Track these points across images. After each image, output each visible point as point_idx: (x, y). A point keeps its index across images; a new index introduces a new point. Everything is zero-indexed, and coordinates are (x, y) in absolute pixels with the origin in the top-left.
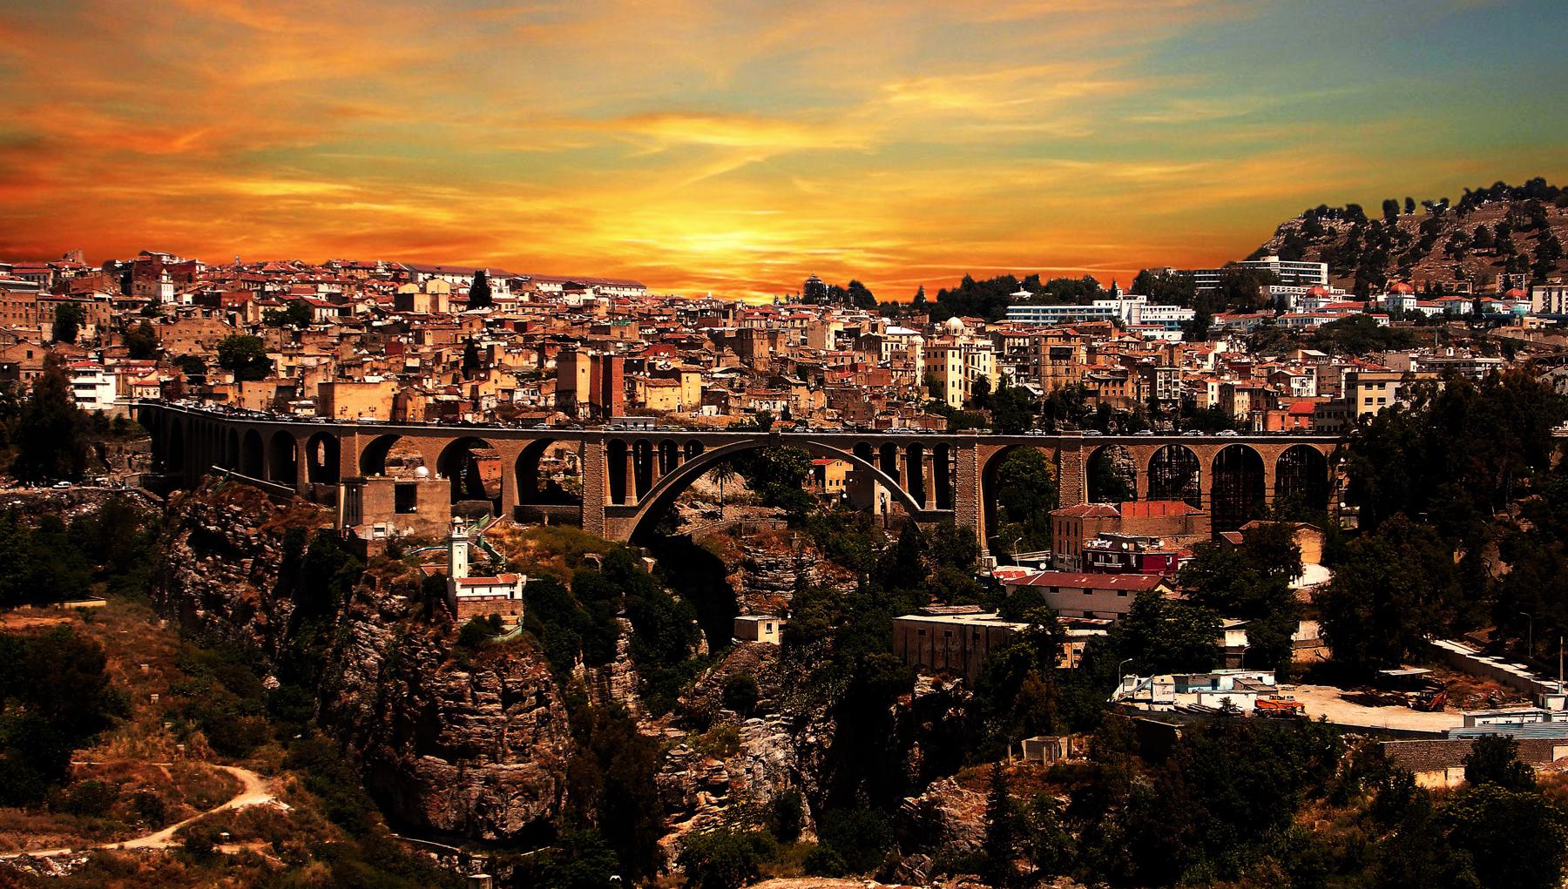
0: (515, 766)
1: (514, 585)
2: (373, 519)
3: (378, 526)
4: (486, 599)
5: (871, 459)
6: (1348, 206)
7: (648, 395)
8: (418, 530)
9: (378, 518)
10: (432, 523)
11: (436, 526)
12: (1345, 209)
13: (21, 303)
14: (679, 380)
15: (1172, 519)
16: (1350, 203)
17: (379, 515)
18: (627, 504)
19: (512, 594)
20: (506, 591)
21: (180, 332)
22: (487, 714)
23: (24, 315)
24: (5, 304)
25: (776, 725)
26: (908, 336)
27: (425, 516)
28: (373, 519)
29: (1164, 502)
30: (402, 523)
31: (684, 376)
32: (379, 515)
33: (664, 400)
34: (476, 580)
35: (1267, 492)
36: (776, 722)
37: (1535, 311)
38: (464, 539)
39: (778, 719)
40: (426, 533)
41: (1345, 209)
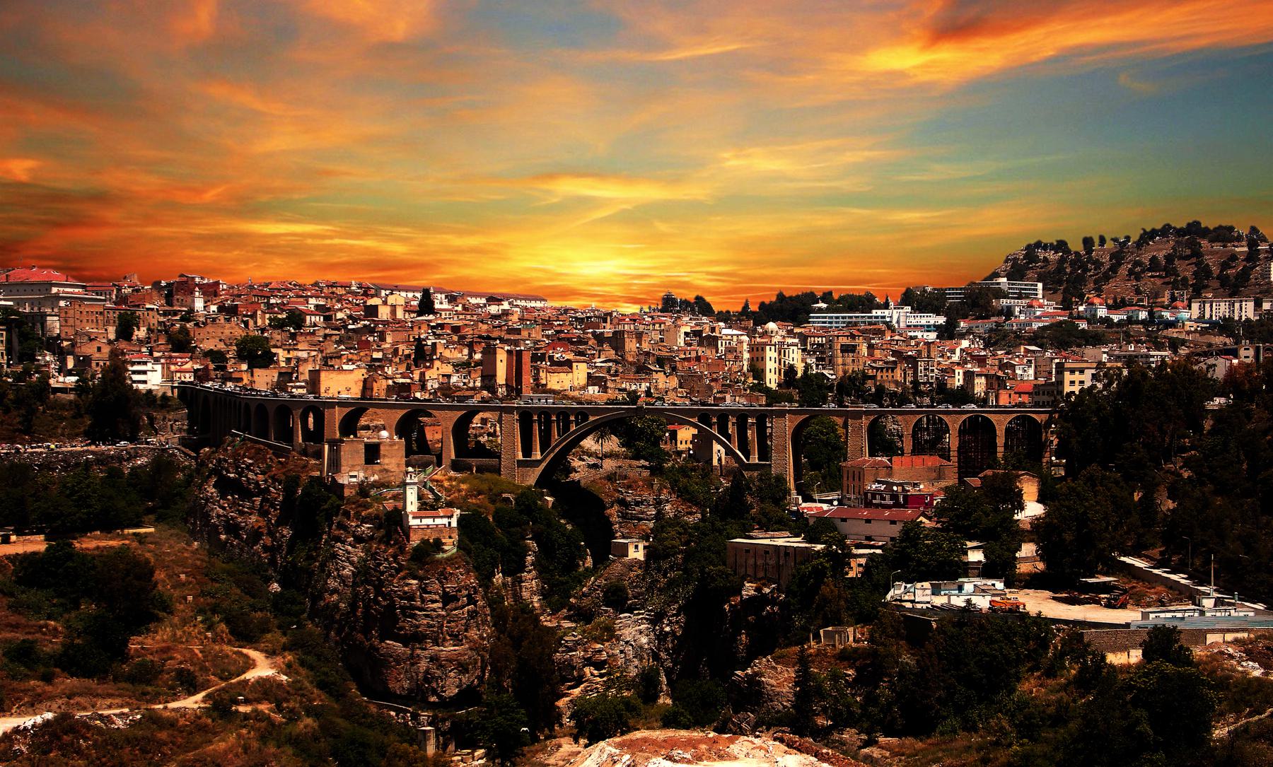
0: (452, 648)
1: (451, 517)
3: (352, 474)
7: (549, 379)
8: (381, 477)
9: (353, 467)
10: (392, 472)
12: (1055, 243)
14: (571, 367)
16: (1059, 239)
17: (353, 466)
19: (450, 523)
20: (445, 521)
22: (431, 610)
24: (81, 312)
25: (641, 619)
27: (386, 467)
30: (369, 472)
32: (353, 466)
34: (423, 513)
38: (414, 484)
39: (643, 614)
40: (387, 479)
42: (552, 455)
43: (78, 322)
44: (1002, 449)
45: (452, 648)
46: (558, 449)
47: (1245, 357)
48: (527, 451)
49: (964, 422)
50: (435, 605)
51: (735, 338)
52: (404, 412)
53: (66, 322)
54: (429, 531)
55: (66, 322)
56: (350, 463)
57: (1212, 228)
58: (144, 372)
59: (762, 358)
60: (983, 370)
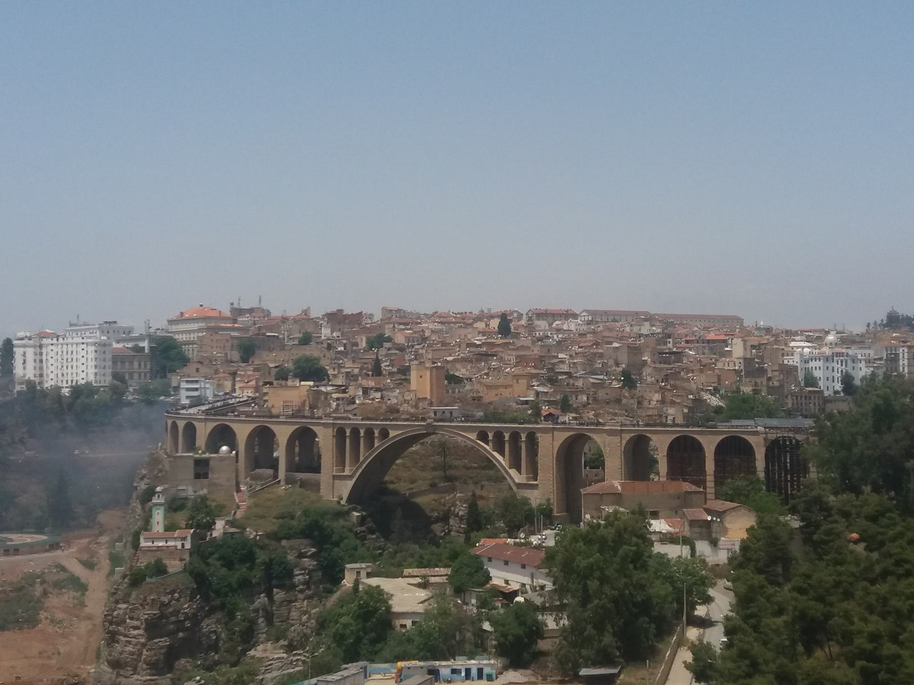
0: (149, 678)
1: (184, 539)
5: (487, 443)
6: (385, 310)
10: (222, 486)
12: (66, 392)
16: (393, 305)
19: (183, 545)
20: (179, 544)
21: (293, 354)
22: (133, 637)
24: (212, 340)
25: (297, 660)
27: (216, 481)
34: (169, 534)
35: (708, 478)
36: (299, 657)
37: (774, 599)
38: (160, 504)
39: (300, 655)
41: (66, 392)
42: (360, 471)
44: (712, 484)
45: (149, 678)
46: (364, 465)
48: (341, 462)
49: (723, 440)
50: (136, 632)
52: (297, 427)
57: (689, 547)
59: (8, 555)
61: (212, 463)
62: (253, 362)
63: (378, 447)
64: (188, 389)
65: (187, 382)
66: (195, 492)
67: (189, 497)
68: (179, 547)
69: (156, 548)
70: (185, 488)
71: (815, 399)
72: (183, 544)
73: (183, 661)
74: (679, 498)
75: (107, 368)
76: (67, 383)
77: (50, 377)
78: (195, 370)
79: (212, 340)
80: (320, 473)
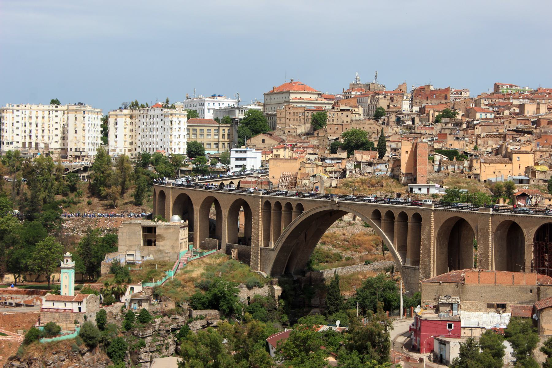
2: (127, 248)
3: (129, 253)
4: (60, 311)
7: (483, 169)
8: (157, 257)
9: (130, 247)
10: (166, 253)
11: (169, 255)
13: (297, 113)
14: (511, 159)
15: (521, 289)
17: (131, 246)
18: (269, 247)
19: (80, 308)
23: (299, 120)
24: (290, 113)
26: (513, 134)
27: (161, 248)
28: (127, 248)
29: (513, 273)
30: (145, 252)
31: (515, 156)
32: (131, 246)
33: (497, 173)
40: (162, 259)
43: (287, 121)
47: (25, 132)
48: (267, 244)
51: (47, 112)
53: (280, 121)
54: (57, 315)
55: (280, 121)
56: (128, 243)
58: (245, 159)
60: (324, 163)
61: (158, 232)
62: (318, 134)
63: (295, 222)
64: (237, 159)
65: (237, 152)
66: (143, 257)
67: (137, 262)
68: (76, 310)
69: (55, 310)
70: (134, 254)
71: (30, 143)
72: (80, 308)
73: (311, 352)
74: (531, 291)
75: (182, 136)
76: (153, 151)
77: (138, 145)
78: (261, 141)
79: (290, 113)
80: (118, 251)
